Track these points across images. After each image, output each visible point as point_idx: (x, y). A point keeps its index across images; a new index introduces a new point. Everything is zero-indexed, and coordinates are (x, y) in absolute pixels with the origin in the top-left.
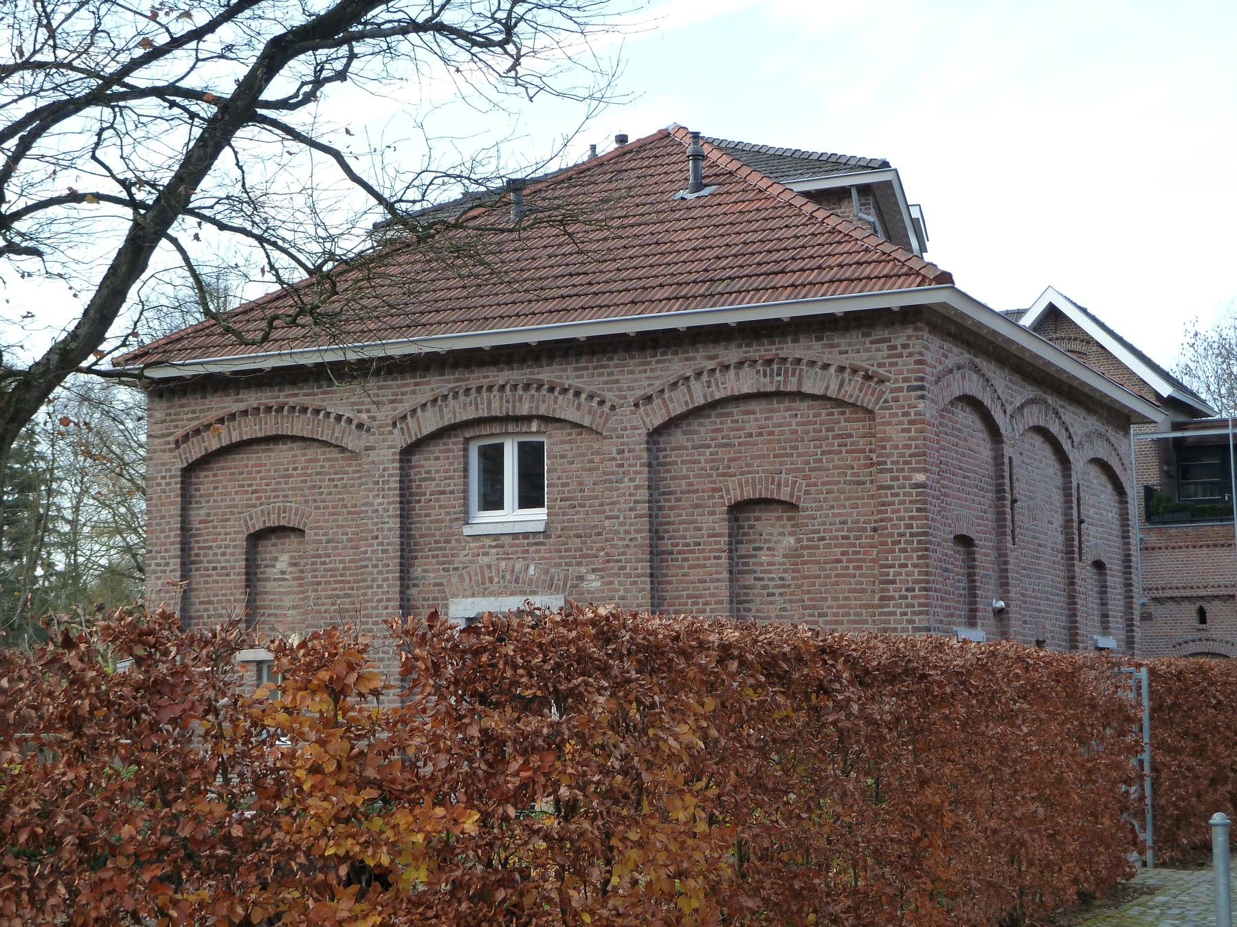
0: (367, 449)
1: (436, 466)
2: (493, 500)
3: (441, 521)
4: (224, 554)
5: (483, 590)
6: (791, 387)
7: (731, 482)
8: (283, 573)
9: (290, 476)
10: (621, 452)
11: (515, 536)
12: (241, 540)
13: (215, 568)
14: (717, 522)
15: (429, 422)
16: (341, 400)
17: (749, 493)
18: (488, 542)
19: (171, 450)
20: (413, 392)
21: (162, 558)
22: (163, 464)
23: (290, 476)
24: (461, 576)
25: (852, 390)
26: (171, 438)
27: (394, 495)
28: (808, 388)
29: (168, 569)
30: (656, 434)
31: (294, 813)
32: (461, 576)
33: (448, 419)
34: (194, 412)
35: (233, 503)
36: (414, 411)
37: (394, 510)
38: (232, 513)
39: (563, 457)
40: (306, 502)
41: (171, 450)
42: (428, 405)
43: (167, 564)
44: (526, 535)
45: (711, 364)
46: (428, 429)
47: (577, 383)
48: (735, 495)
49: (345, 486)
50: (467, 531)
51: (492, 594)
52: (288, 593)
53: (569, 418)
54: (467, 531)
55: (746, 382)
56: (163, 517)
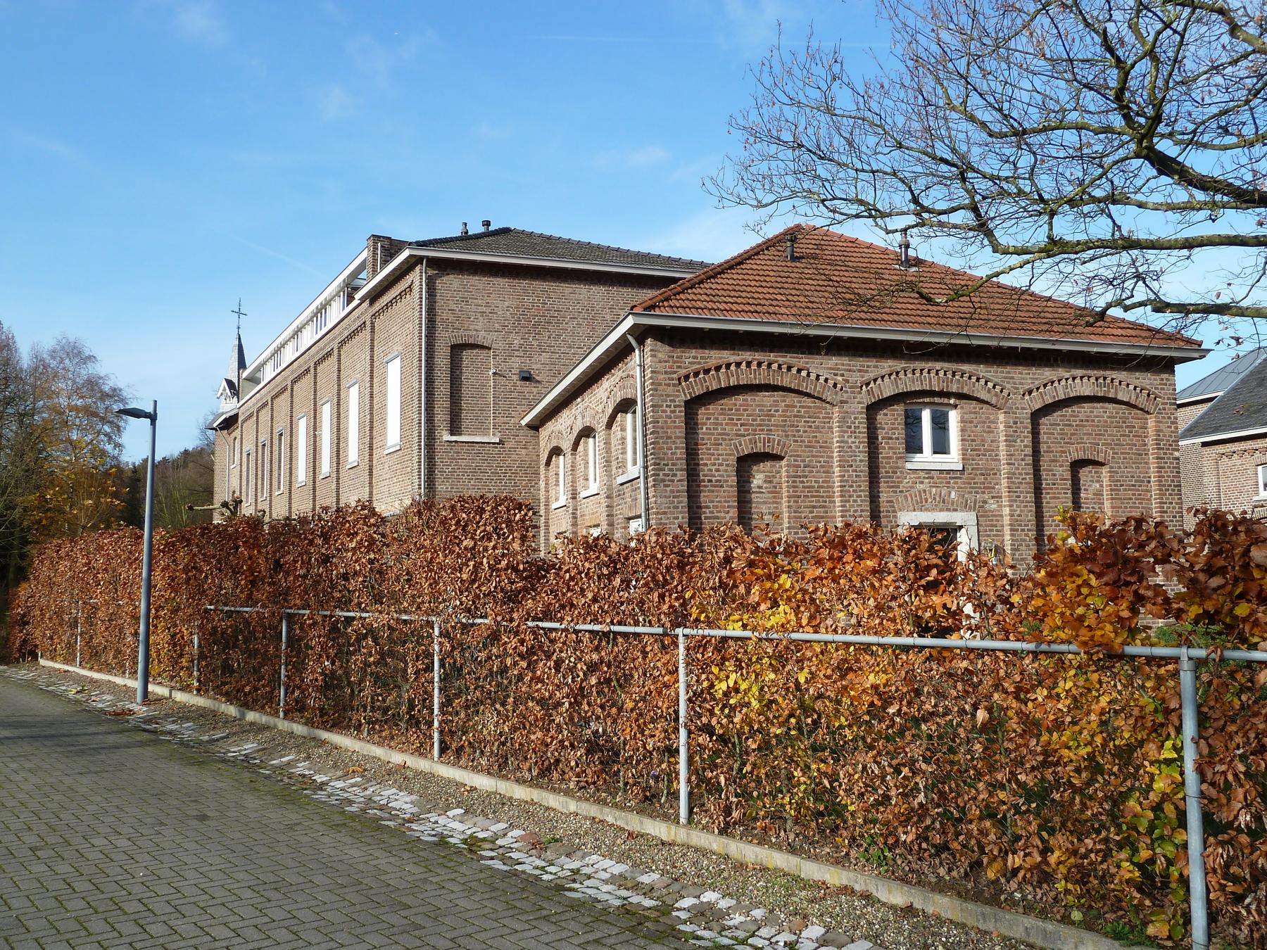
0: (842, 402)
1: (891, 420)
2: (914, 446)
3: (890, 458)
4: (718, 470)
5: (920, 506)
6: (1111, 395)
7: (1072, 448)
8: (760, 487)
9: (773, 416)
10: (1015, 423)
11: (941, 471)
12: (732, 461)
13: (710, 481)
14: (1063, 472)
15: (888, 389)
16: (823, 367)
17: (1081, 456)
18: (922, 474)
19: (674, 385)
20: (876, 367)
21: (671, 470)
22: (668, 396)
23: (773, 416)
24: (906, 497)
25: (1142, 401)
26: (675, 376)
27: (864, 437)
28: (1120, 397)
29: (676, 479)
30: (1037, 416)
31: (1170, 667)
32: (906, 497)
33: (902, 388)
34: (695, 357)
35: (725, 433)
36: (696, 374)
37: (863, 447)
38: (724, 440)
39: (971, 422)
40: (787, 436)
41: (674, 385)
42: (890, 377)
43: (675, 475)
44: (949, 471)
45: (1067, 375)
46: (887, 393)
47: (988, 375)
48: (1075, 456)
49: (817, 427)
50: (909, 466)
51: (927, 510)
52: (765, 503)
53: (983, 397)
54: (909, 466)
55: (1086, 388)
56: (670, 438)
